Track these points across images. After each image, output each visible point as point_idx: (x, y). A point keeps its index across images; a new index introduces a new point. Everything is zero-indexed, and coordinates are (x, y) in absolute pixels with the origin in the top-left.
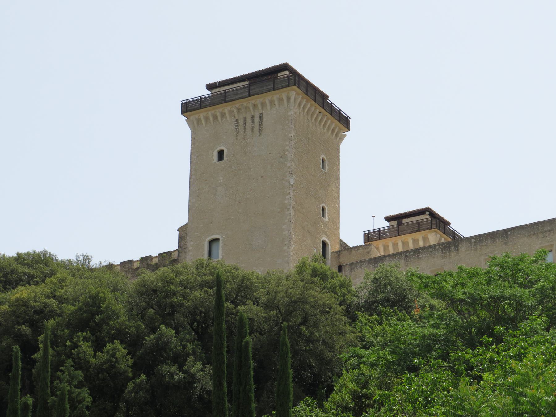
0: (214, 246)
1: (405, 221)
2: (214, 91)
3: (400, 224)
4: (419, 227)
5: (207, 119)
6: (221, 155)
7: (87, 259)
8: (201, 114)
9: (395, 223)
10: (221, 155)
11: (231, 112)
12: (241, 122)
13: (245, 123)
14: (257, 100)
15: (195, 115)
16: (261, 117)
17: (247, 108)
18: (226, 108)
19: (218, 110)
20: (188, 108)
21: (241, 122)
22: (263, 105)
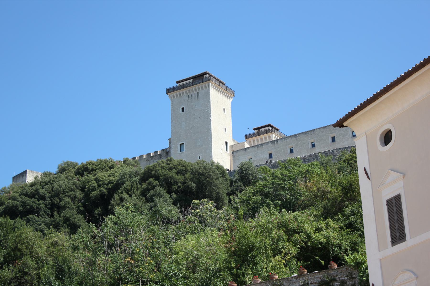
0: (182, 146)
1: (261, 130)
2: (179, 84)
3: (259, 131)
4: (266, 132)
5: (177, 95)
6: (183, 109)
7: (425, 59)
8: (174, 93)
9: (257, 131)
10: (183, 109)
11: (186, 92)
12: (190, 96)
13: (192, 96)
14: (196, 86)
15: (172, 94)
16: (198, 94)
17: (192, 90)
18: (184, 90)
19: (181, 91)
20: (169, 91)
21: (190, 96)
22: (199, 88)
